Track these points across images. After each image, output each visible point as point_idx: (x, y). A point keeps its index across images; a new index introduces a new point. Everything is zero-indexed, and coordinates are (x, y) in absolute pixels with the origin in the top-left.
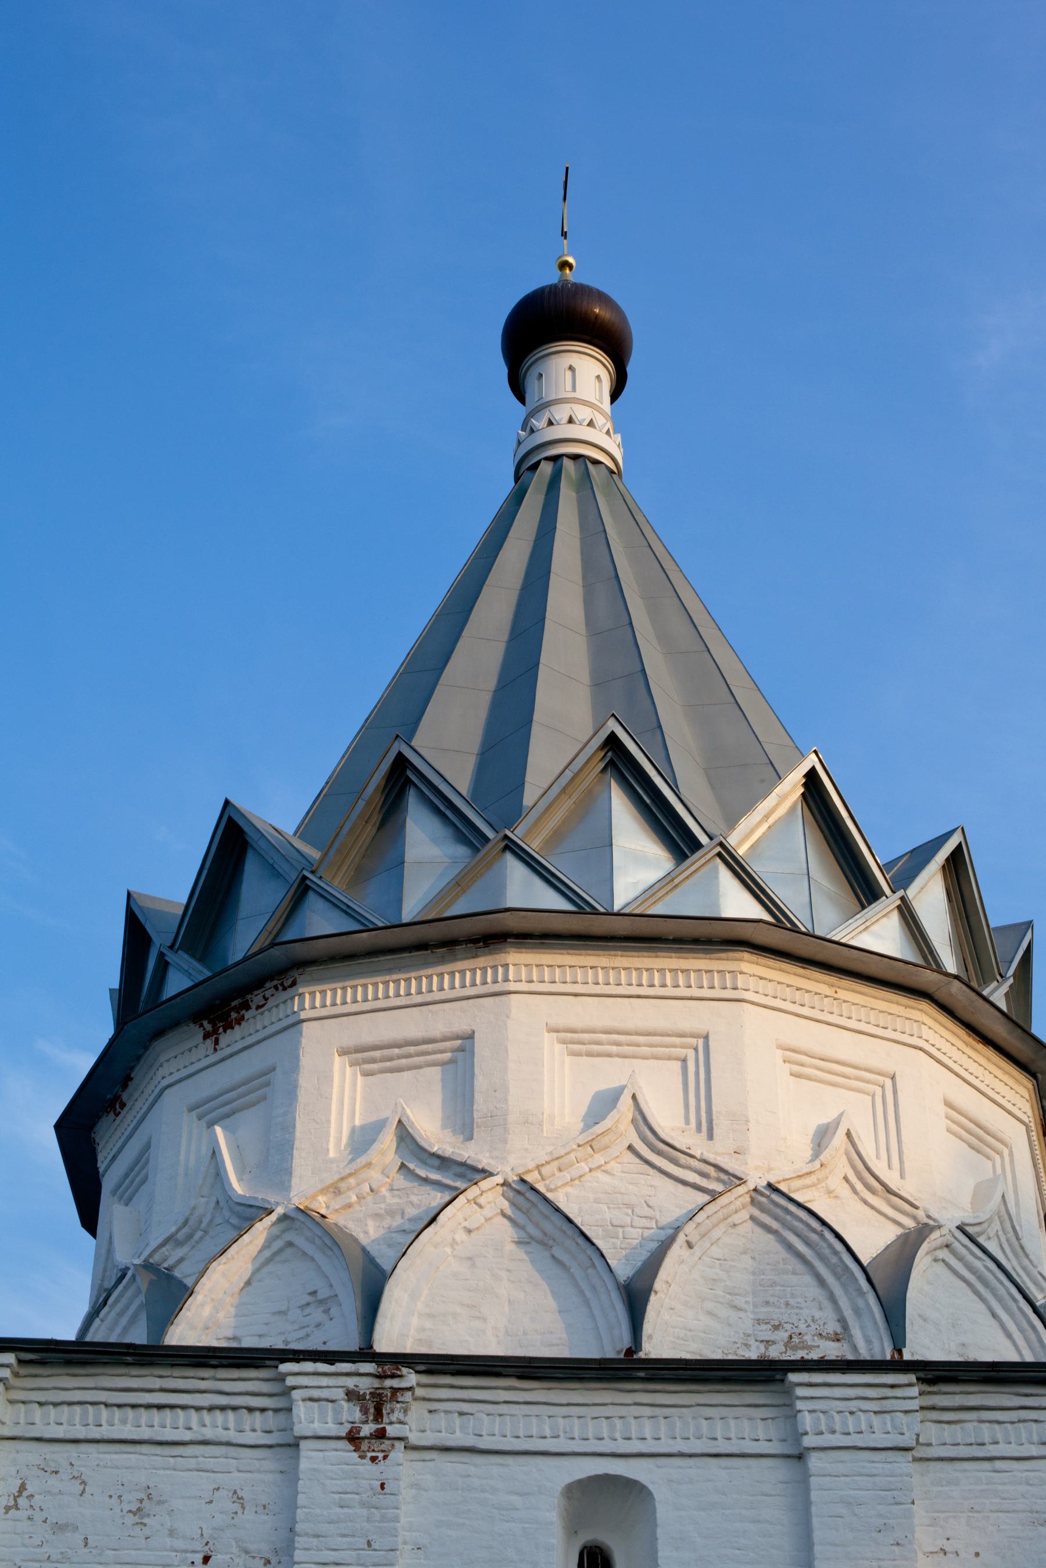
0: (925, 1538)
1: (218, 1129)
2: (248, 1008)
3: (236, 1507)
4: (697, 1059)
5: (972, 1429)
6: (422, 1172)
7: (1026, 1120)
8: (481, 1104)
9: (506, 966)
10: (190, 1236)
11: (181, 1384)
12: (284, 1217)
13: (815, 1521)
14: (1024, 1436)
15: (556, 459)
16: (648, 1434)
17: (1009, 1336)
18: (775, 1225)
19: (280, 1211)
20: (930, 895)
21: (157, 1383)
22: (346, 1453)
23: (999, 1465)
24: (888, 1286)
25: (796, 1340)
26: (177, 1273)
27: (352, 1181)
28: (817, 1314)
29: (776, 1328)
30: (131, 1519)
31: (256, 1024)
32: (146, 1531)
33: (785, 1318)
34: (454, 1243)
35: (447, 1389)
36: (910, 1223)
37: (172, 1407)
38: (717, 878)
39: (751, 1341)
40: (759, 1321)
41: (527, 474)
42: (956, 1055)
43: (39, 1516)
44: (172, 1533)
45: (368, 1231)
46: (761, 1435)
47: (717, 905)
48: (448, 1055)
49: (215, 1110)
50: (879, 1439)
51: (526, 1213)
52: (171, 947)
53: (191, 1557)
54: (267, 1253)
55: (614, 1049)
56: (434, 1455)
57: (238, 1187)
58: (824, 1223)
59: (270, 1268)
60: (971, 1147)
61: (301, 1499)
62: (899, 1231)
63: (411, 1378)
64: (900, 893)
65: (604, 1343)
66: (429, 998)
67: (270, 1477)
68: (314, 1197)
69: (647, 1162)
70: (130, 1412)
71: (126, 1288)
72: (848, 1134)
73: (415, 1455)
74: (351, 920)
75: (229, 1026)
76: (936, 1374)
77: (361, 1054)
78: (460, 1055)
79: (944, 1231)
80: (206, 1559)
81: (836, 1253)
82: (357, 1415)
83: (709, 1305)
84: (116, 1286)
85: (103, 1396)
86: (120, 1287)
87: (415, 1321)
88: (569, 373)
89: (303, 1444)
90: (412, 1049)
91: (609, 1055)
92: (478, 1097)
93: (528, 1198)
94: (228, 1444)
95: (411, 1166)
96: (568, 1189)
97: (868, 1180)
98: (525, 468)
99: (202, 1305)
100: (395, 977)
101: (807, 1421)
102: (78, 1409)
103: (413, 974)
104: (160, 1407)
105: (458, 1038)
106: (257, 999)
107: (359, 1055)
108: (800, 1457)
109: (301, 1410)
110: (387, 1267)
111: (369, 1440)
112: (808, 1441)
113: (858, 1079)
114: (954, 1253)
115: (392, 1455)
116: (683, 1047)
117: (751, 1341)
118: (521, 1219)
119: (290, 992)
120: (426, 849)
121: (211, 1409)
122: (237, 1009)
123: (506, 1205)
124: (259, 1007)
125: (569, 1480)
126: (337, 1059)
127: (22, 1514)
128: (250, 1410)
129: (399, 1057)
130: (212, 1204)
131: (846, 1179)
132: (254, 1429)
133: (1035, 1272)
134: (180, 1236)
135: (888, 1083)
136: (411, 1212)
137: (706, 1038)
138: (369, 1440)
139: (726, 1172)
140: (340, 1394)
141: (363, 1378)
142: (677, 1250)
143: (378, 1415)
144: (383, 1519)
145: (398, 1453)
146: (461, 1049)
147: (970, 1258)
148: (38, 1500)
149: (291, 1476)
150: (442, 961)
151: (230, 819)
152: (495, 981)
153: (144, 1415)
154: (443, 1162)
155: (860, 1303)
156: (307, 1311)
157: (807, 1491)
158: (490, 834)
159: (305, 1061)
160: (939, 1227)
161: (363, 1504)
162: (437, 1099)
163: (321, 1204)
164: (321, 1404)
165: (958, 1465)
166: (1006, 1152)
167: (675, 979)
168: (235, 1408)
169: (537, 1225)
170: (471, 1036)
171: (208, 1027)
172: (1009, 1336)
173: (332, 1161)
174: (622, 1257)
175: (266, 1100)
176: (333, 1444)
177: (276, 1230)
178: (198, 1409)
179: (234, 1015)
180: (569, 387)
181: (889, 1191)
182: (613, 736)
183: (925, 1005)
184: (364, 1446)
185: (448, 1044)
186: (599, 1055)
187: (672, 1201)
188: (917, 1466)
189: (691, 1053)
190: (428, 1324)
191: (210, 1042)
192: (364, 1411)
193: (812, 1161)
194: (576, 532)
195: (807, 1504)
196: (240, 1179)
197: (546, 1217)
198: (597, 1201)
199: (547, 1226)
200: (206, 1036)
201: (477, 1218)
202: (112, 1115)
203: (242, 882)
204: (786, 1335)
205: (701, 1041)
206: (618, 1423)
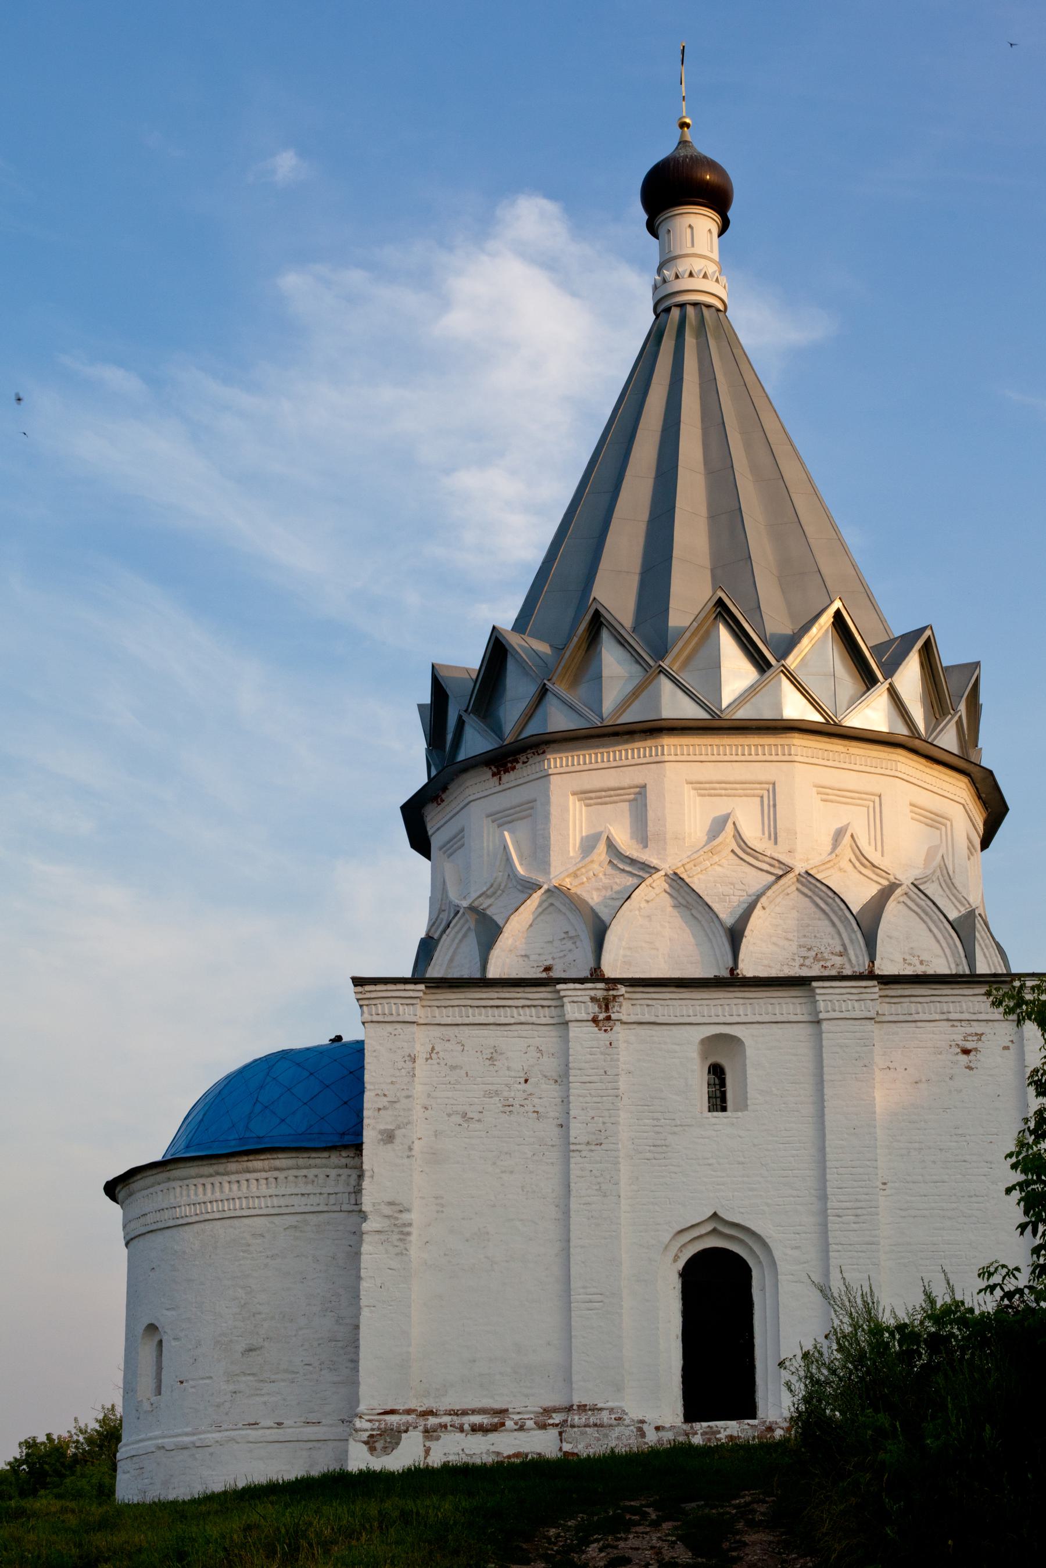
0: (879, 1061)
1: (506, 833)
2: (518, 762)
3: (539, 1055)
4: (770, 801)
5: (906, 1007)
6: (621, 866)
7: (963, 801)
8: (651, 828)
9: (662, 746)
10: (494, 893)
11: (507, 995)
12: (548, 890)
13: (824, 1055)
14: (933, 1009)
15: (682, 306)
16: (741, 1013)
17: (938, 941)
18: (810, 893)
19: (545, 887)
20: (909, 678)
21: (496, 995)
22: (593, 1028)
23: (919, 1024)
24: (868, 925)
25: (819, 956)
26: (488, 912)
27: (583, 870)
28: (831, 942)
29: (809, 949)
30: (488, 1062)
31: (522, 773)
32: (496, 1068)
33: (814, 944)
34: (640, 909)
35: (640, 993)
36: (886, 883)
37: (504, 1006)
38: (780, 686)
39: (796, 958)
40: (800, 946)
41: (663, 315)
42: (919, 774)
43: (442, 1063)
44: (508, 1068)
45: (594, 899)
46: (798, 1011)
47: (779, 706)
48: (632, 796)
49: (503, 819)
50: (858, 1014)
51: (678, 891)
52: (466, 711)
53: (519, 1080)
54: (540, 910)
55: (723, 792)
56: (635, 1026)
57: (521, 870)
58: (835, 893)
59: (542, 917)
60: (927, 825)
61: (571, 1051)
62: (879, 887)
63: (622, 990)
64: (889, 680)
66: (620, 763)
67: (554, 1039)
68: (563, 880)
69: (742, 859)
70: (483, 1010)
71: (460, 919)
72: (852, 836)
73: (626, 1026)
74: (575, 716)
75: (506, 771)
77: (585, 795)
78: (639, 796)
79: (904, 887)
80: (526, 1081)
81: (841, 909)
82: (597, 1009)
83: (774, 939)
84: (454, 918)
85: (469, 1002)
86: (457, 918)
87: (621, 952)
88: (689, 231)
89: (570, 1024)
90: (612, 793)
91: (721, 796)
92: (650, 823)
93: (677, 882)
94: (533, 1024)
95: (615, 862)
96: (700, 876)
97: (862, 859)
98: (661, 310)
99: (507, 939)
100: (601, 750)
101: (821, 1005)
102: (456, 1009)
103: (611, 749)
104: (497, 1007)
105: (637, 787)
106: (523, 758)
107: (583, 796)
108: (819, 1022)
109: (568, 1008)
111: (603, 1021)
112: (822, 1016)
113: (859, 799)
114: (909, 897)
115: (615, 1028)
116: (762, 789)
117: (796, 958)
118: (675, 894)
119: (542, 756)
120: (614, 665)
121: (523, 1007)
122: (512, 762)
123: (667, 886)
124: (524, 763)
125: (703, 1037)
126: (571, 797)
127: (434, 1062)
128: (543, 1006)
129: (605, 797)
130: (506, 877)
131: (850, 861)
132: (545, 1016)
133: (960, 896)
134: (489, 893)
135: (877, 799)
136: (616, 888)
137: (774, 784)
139: (784, 864)
140: (588, 999)
141: (598, 990)
142: (757, 912)
143: (607, 1009)
144: (612, 1060)
145: (618, 1027)
146: (639, 793)
147: (918, 900)
148: (441, 1054)
149: (565, 1039)
150: (627, 742)
151: (497, 639)
152: (657, 755)
153: (490, 1011)
154: (633, 861)
155: (854, 937)
156: (564, 942)
157: (821, 1040)
158: (651, 663)
159: (554, 798)
160: (900, 885)
161: (602, 1053)
162: (627, 821)
163: (568, 883)
164: (578, 1003)
165: (899, 1025)
166: (948, 823)
167: (757, 750)
168: (534, 1006)
169: (683, 897)
170: (644, 787)
171: (495, 770)
172: (938, 941)
173: (572, 858)
174: (727, 914)
175: (533, 815)
176: (585, 1024)
177: (544, 897)
178: (517, 1007)
179: (509, 765)
180: (689, 244)
181: (874, 866)
182: (720, 599)
183: (900, 751)
184: (601, 1024)
185: (632, 790)
186: (715, 795)
187: (756, 880)
188: (877, 1025)
189: (765, 793)
190: (628, 953)
191: (496, 778)
192: (600, 1007)
193: (831, 853)
194: (696, 390)
195: (821, 1047)
196: (521, 864)
197: (676, 1259)
198: (715, 882)
199: (690, 900)
200: (494, 775)
201: (652, 894)
202: (435, 804)
203: (505, 677)
204: (814, 954)
205: (771, 786)
206: (727, 1008)
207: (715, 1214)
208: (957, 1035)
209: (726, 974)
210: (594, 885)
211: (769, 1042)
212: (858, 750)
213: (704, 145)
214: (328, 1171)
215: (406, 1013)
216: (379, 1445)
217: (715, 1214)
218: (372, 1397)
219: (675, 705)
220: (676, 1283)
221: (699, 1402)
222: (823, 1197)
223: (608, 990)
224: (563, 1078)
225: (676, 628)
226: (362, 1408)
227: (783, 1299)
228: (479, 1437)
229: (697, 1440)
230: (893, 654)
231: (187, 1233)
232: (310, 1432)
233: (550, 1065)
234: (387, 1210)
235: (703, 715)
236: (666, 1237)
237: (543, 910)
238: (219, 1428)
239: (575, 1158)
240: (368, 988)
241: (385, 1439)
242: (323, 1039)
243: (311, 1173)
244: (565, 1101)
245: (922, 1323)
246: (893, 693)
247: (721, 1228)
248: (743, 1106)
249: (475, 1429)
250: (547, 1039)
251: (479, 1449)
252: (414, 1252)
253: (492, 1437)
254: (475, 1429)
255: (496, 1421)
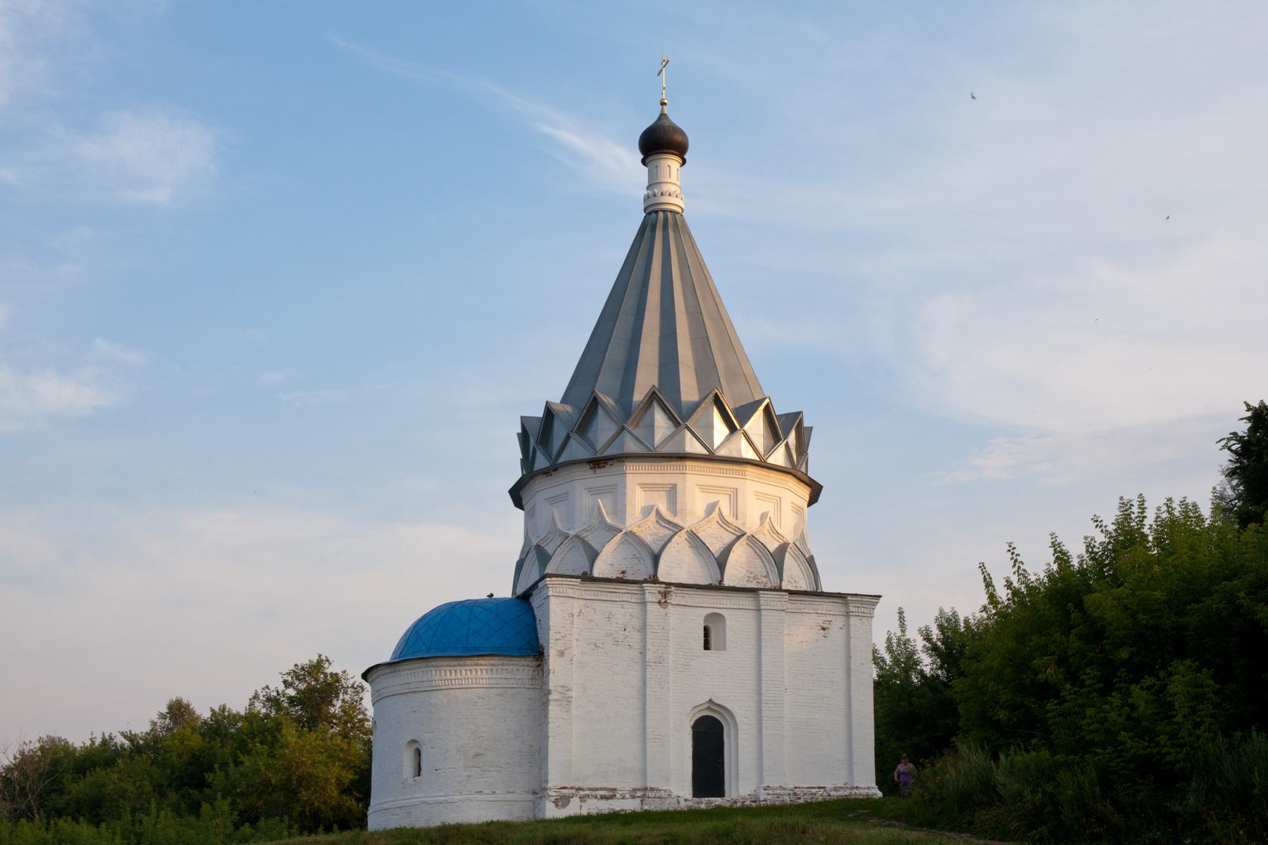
4: (734, 496)
5: (798, 605)
20: (756, 425)
35: (680, 591)
57: (608, 520)
76: (791, 593)
77: (644, 486)
93: (693, 537)
111: (663, 603)
132: (634, 599)
138: (663, 603)
149: (644, 611)
154: (669, 523)
163: (635, 530)
174: (716, 548)
207: (710, 701)
208: (820, 620)
209: (716, 583)
210: (650, 532)
211: (737, 618)
213: (678, 118)
215: (571, 592)
217: (710, 701)
218: (555, 780)
219: (692, 446)
220: (690, 732)
221: (699, 791)
222: (759, 694)
224: (643, 629)
225: (687, 402)
226: (550, 785)
227: (740, 741)
228: (604, 801)
229: (703, 806)
230: (745, 413)
231: (440, 695)
232: (509, 797)
233: (636, 622)
234: (561, 690)
235: (704, 452)
236: (689, 709)
237: (622, 543)
238: (461, 794)
239: (649, 669)
241: (562, 801)
242: (484, 596)
243: (510, 668)
244: (644, 641)
246: (787, 446)
248: (723, 647)
249: (603, 797)
250: (635, 610)
251: (605, 807)
252: (573, 711)
253: (610, 801)
254: (603, 797)
255: (611, 794)
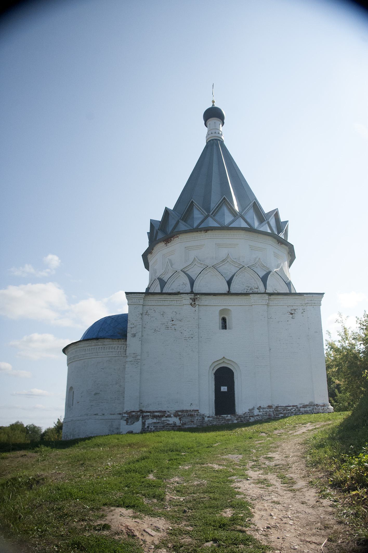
63: (199, 296)
65: (224, 288)
110: (194, 279)
142: (235, 277)
143: (194, 301)
164: (187, 300)
197: (213, 370)
208: (289, 309)
212: (261, 236)
214: (118, 346)
216: (129, 421)
219: (211, 223)
223: (195, 296)
240: (129, 295)
245: (48, 435)
247: (225, 361)
